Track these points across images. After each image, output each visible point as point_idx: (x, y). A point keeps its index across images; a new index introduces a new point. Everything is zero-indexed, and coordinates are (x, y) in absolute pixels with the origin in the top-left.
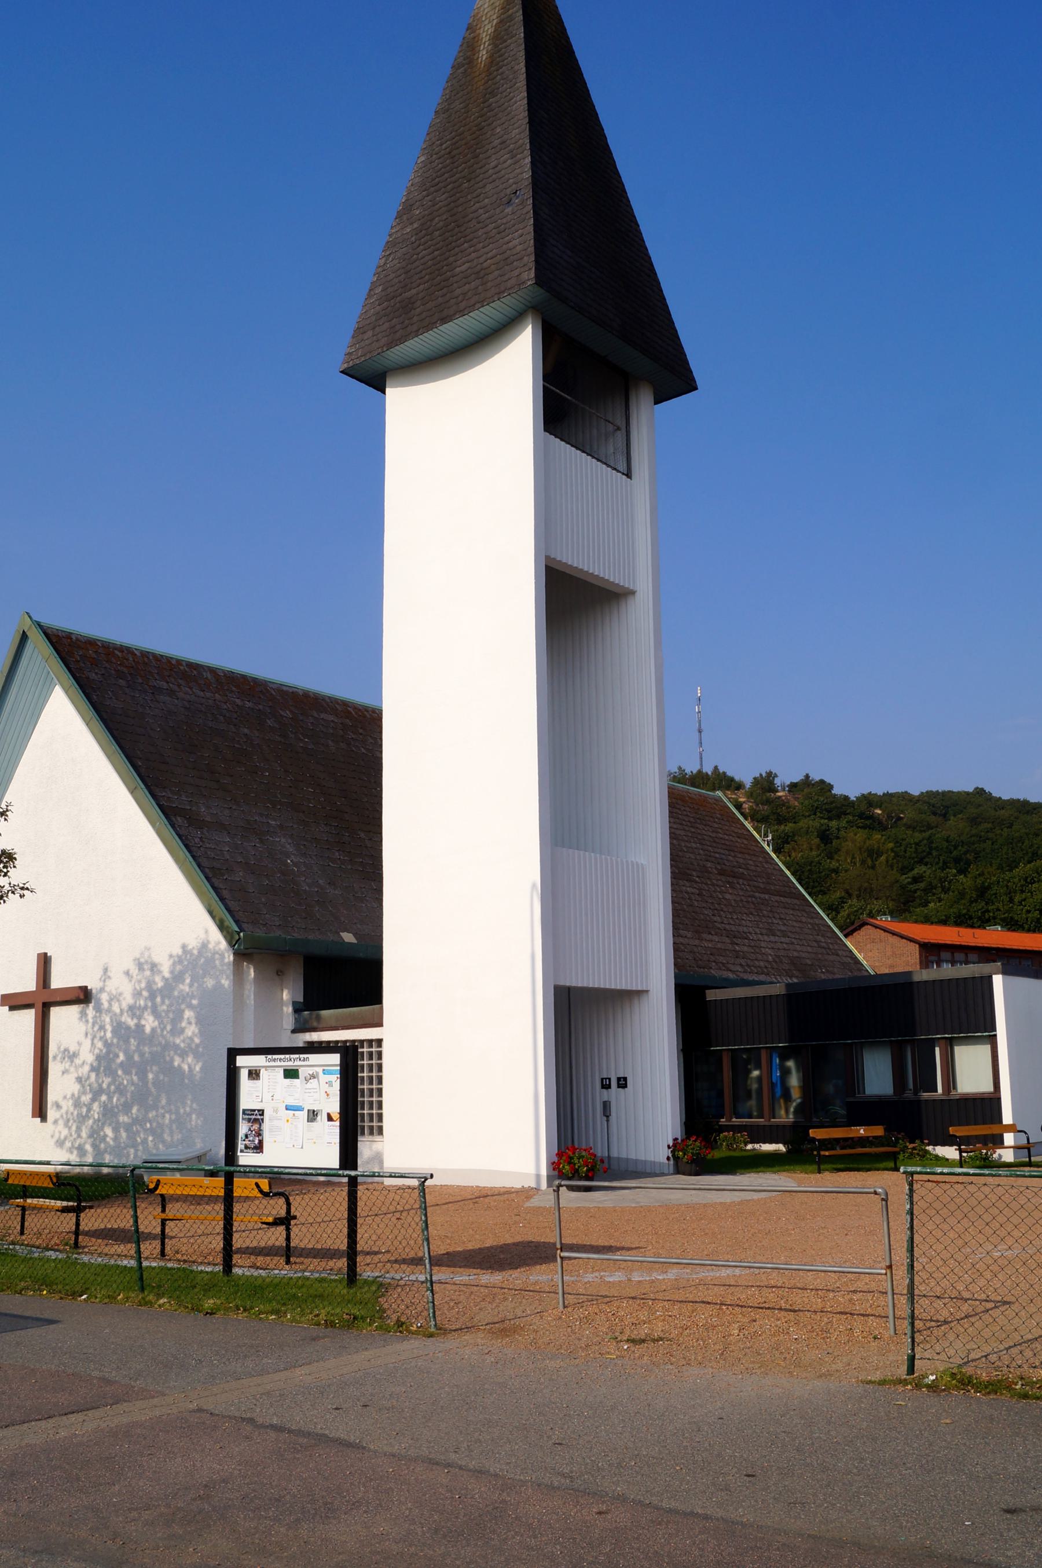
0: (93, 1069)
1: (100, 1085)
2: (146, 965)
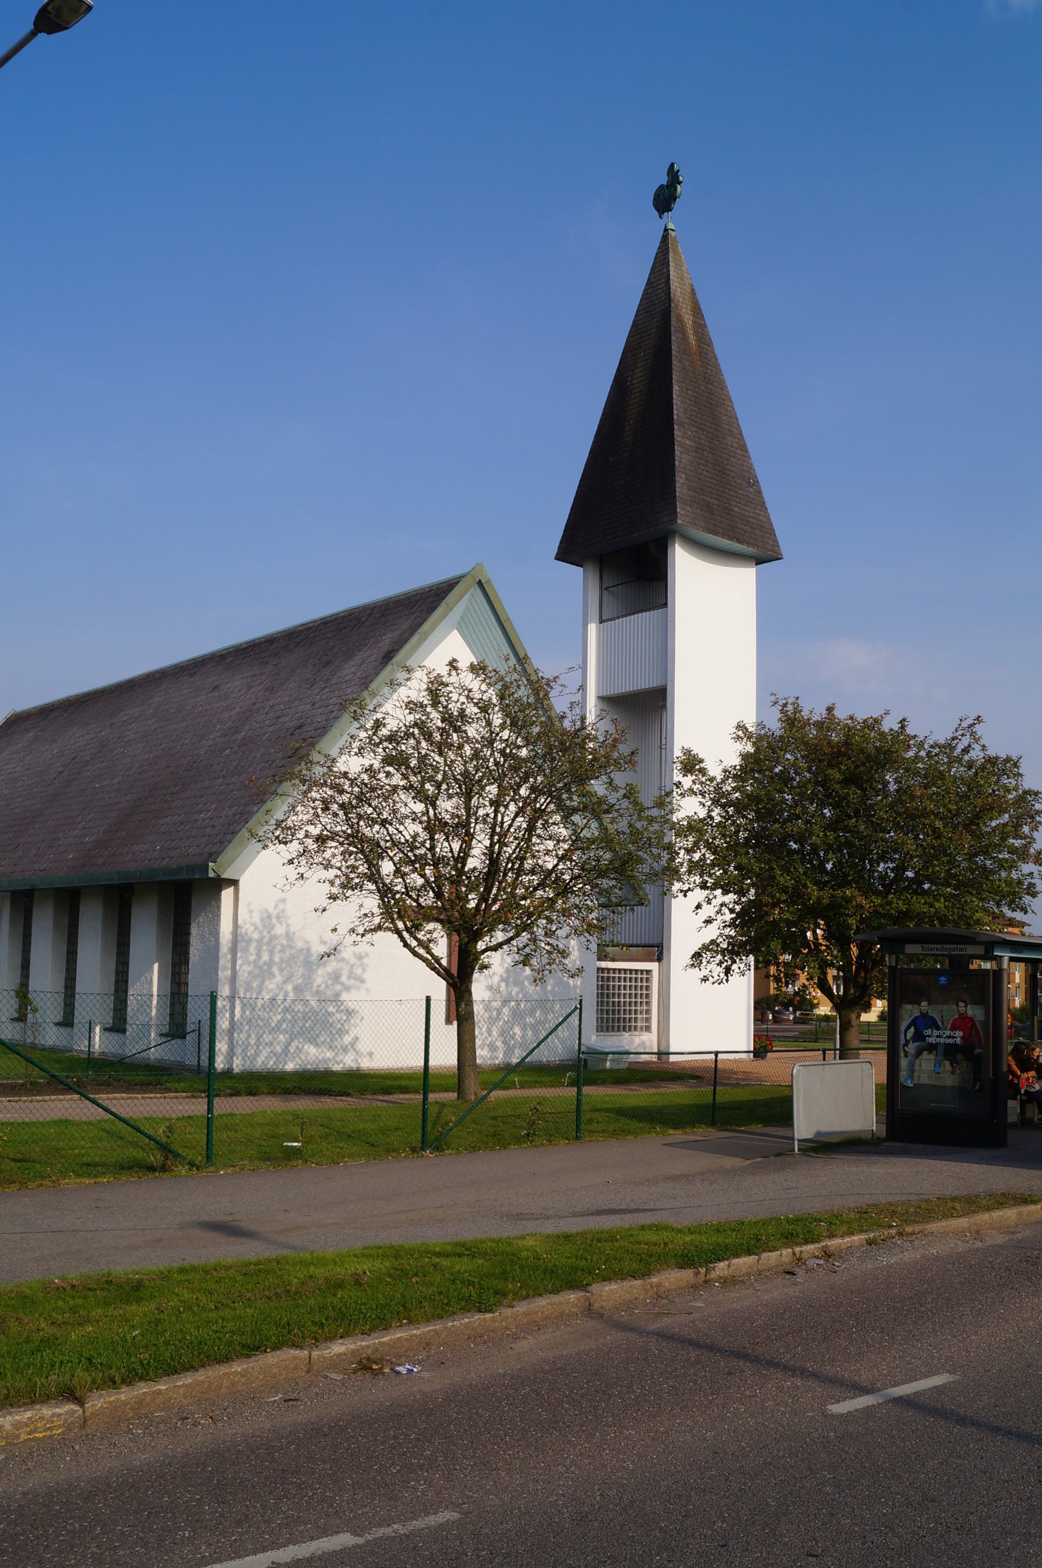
0: (502, 979)
1: (510, 993)
2: (780, 720)
